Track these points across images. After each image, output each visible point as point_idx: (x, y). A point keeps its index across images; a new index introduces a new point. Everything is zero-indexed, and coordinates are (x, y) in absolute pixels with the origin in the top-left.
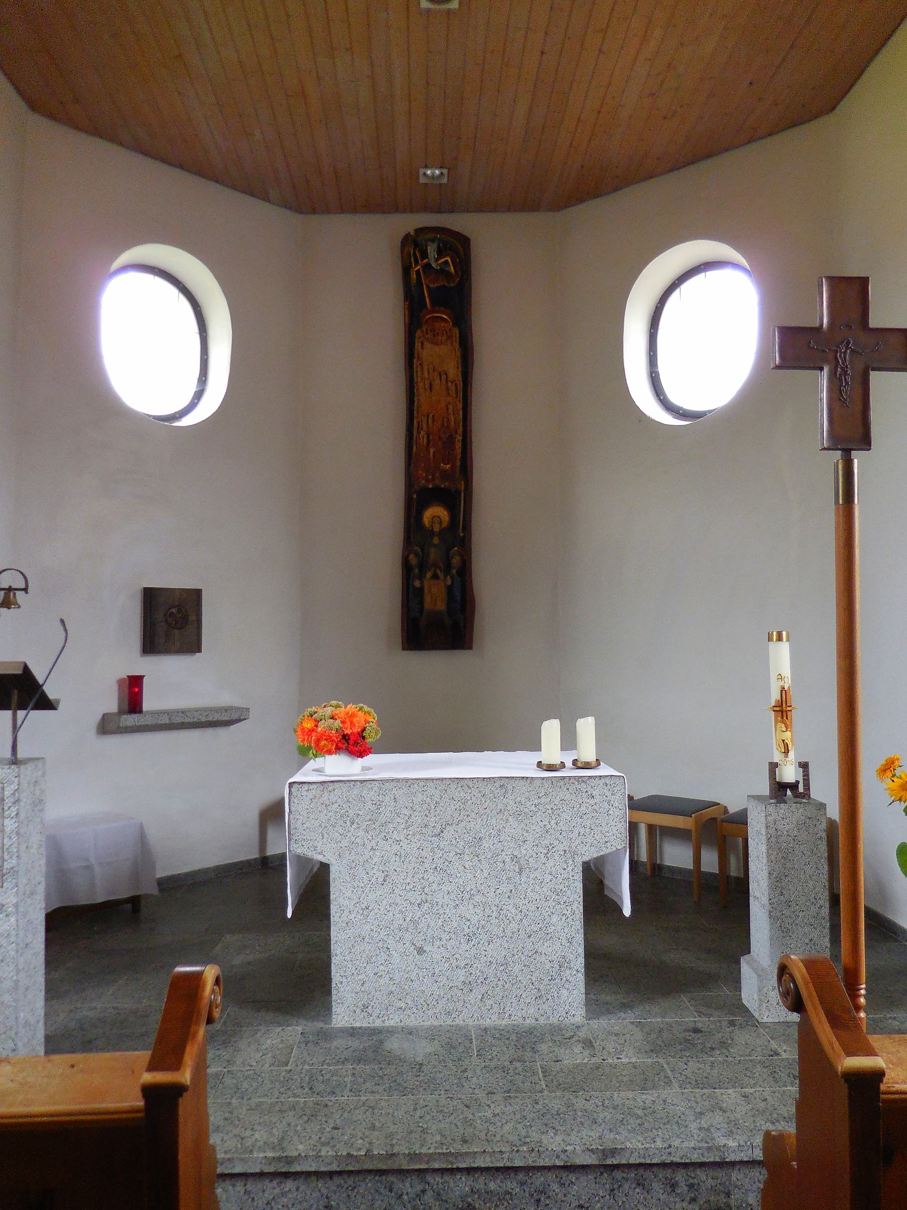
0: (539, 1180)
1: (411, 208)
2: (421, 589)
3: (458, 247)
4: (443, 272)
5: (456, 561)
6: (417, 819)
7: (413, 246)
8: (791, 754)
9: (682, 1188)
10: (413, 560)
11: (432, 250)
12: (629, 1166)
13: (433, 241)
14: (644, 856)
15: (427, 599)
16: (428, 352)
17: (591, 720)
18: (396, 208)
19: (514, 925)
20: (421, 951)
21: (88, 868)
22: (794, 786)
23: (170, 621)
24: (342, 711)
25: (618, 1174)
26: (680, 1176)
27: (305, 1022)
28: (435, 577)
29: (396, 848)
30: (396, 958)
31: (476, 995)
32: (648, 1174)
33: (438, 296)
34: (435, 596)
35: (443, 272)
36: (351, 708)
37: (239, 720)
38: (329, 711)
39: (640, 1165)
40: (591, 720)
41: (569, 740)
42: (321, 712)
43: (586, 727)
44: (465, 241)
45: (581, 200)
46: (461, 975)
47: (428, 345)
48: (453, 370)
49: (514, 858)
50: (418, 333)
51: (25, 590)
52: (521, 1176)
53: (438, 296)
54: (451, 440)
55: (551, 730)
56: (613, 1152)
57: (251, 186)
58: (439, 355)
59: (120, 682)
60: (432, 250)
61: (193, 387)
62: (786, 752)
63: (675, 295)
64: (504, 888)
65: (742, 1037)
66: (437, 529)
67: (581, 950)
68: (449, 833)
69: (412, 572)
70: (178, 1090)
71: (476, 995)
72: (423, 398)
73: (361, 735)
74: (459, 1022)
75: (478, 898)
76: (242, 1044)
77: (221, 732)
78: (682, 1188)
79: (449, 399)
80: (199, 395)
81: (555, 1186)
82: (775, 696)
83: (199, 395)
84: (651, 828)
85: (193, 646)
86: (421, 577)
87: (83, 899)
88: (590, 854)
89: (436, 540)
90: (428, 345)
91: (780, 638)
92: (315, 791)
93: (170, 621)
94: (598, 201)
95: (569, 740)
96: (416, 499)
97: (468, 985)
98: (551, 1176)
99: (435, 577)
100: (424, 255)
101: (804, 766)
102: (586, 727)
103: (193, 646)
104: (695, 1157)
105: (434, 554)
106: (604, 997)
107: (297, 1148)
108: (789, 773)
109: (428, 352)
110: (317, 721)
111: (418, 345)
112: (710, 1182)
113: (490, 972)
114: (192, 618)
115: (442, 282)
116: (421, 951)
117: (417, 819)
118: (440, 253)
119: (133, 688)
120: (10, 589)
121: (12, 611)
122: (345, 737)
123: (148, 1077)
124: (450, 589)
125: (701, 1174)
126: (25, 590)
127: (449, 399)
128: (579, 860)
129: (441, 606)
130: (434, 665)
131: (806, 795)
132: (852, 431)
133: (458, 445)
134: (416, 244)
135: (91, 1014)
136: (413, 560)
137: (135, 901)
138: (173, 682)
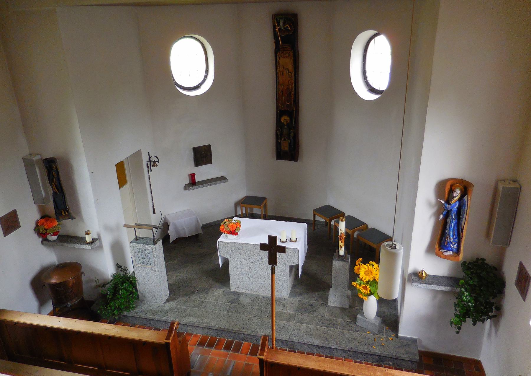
4: (286, 29)
5: (292, 134)
6: (248, 252)
7: (276, 18)
13: (281, 18)
15: (282, 147)
16: (282, 61)
20: (250, 279)
21: (184, 229)
23: (202, 155)
27: (225, 288)
28: (285, 140)
30: (244, 280)
31: (263, 289)
33: (287, 37)
34: (285, 146)
46: (259, 285)
48: (290, 67)
50: (278, 54)
51: (158, 162)
53: (287, 37)
54: (290, 93)
59: (189, 175)
60: (281, 22)
61: (204, 74)
63: (373, 41)
65: (321, 310)
68: (255, 256)
69: (279, 136)
70: (169, 343)
71: (263, 289)
76: (210, 293)
79: (290, 79)
80: (206, 77)
83: (206, 77)
85: (210, 161)
86: (281, 139)
87: (183, 236)
89: (286, 127)
93: (202, 155)
96: (280, 113)
97: (261, 287)
99: (285, 140)
103: (210, 161)
105: (285, 131)
106: (298, 291)
107: (212, 324)
109: (282, 61)
111: (278, 59)
113: (266, 285)
116: (250, 279)
117: (248, 252)
118: (285, 23)
119: (193, 176)
121: (156, 167)
122: (231, 232)
123: (165, 341)
124: (290, 143)
126: (158, 162)
127: (290, 79)
129: (287, 149)
135: (181, 278)
136: (279, 134)
137: (197, 236)
138: (204, 172)
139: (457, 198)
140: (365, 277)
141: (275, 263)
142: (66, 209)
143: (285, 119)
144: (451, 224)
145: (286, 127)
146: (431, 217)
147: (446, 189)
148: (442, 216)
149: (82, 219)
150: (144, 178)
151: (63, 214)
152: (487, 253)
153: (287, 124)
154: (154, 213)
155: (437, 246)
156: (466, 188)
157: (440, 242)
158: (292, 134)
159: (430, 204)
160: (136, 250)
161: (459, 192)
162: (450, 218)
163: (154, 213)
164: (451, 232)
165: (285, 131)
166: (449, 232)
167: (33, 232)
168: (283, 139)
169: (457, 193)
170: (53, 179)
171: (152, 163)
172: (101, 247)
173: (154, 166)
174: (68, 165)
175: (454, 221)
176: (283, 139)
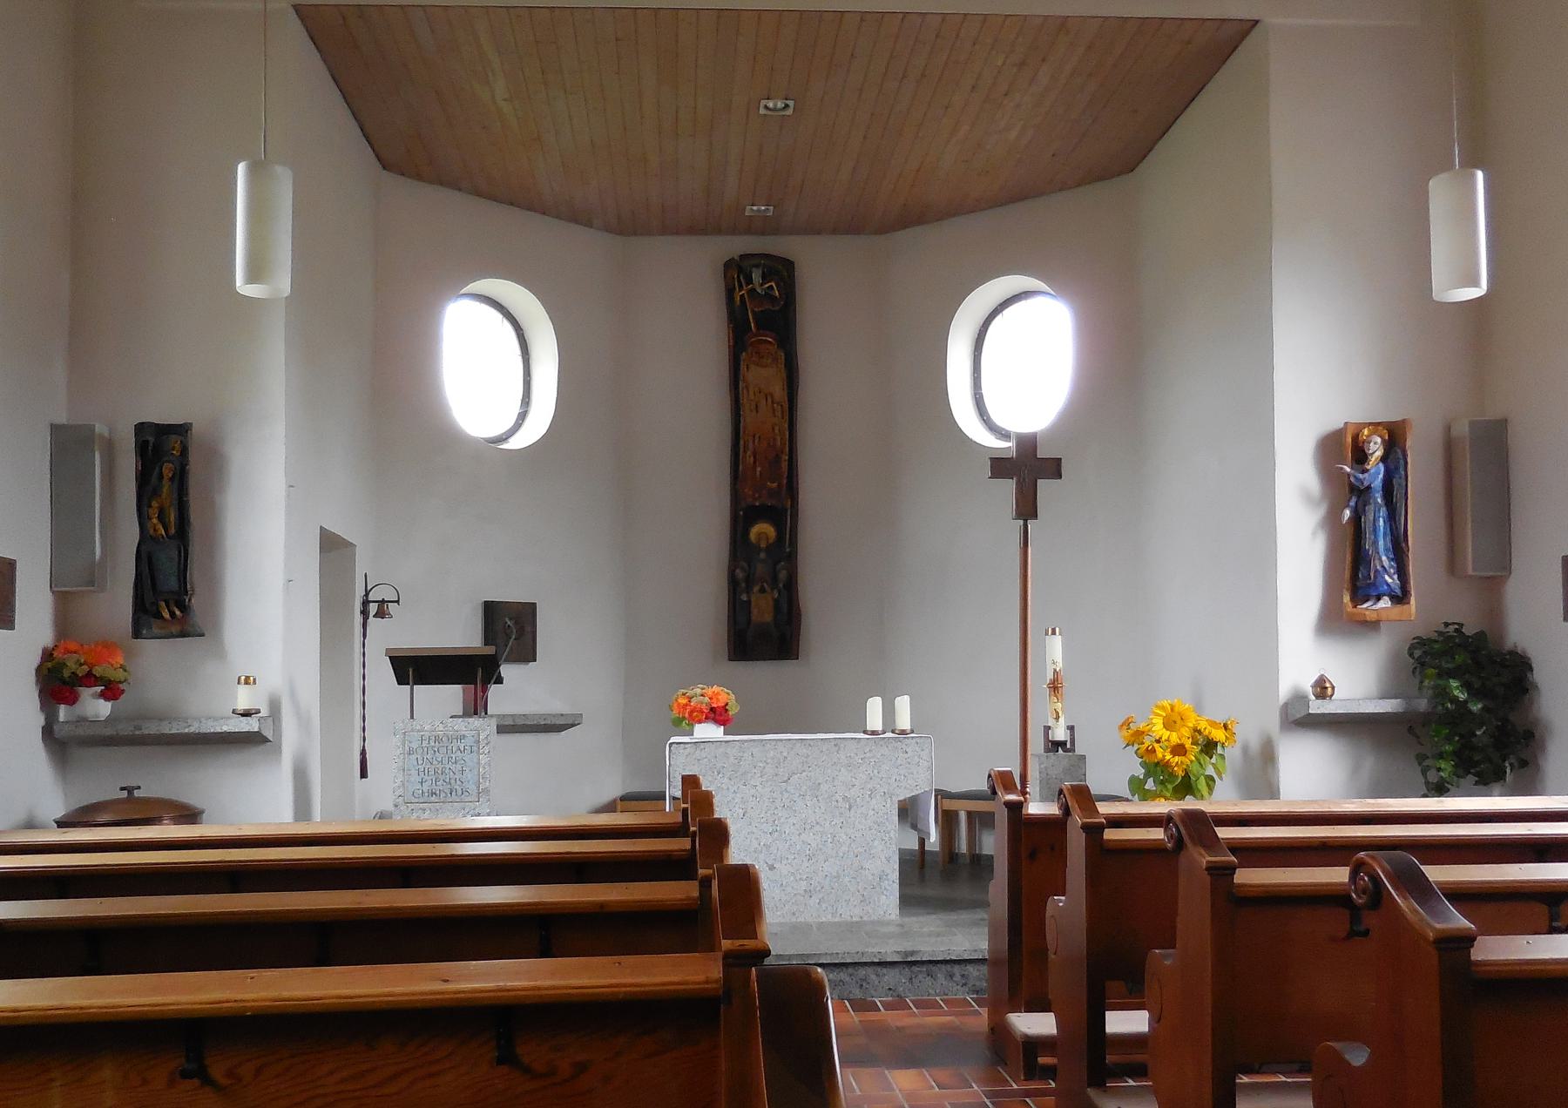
0: (862, 972)
1: (734, 231)
2: (749, 602)
3: (782, 271)
4: (768, 296)
5: (783, 575)
7: (736, 271)
8: (1062, 720)
9: (957, 978)
10: (740, 574)
11: (756, 276)
12: (923, 962)
13: (757, 266)
14: (963, 847)
15: (755, 611)
17: (906, 698)
18: (718, 231)
19: (844, 848)
22: (1062, 744)
24: (709, 691)
25: (916, 969)
26: (957, 969)
28: (762, 590)
29: (753, 791)
31: (815, 900)
32: (934, 968)
33: (761, 317)
34: (762, 608)
35: (768, 296)
36: (716, 688)
37: (573, 725)
38: (698, 691)
39: (930, 962)
40: (906, 698)
41: (889, 713)
42: (690, 693)
43: (903, 704)
44: (789, 265)
45: (905, 227)
47: (752, 367)
48: (779, 391)
49: (845, 798)
52: (850, 970)
53: (761, 317)
54: (778, 458)
55: (875, 707)
56: (912, 953)
57: (577, 216)
58: (764, 377)
60: (756, 276)
61: (516, 409)
62: (1057, 718)
64: (837, 821)
66: (763, 545)
67: (897, 866)
69: (737, 589)
71: (815, 900)
72: (748, 417)
73: (725, 709)
74: (801, 919)
75: (817, 828)
77: (553, 737)
78: (957, 978)
80: (522, 416)
81: (873, 977)
82: (1050, 676)
83: (522, 416)
84: (969, 814)
86: (748, 590)
88: (905, 794)
89: (762, 555)
90: (752, 367)
91: (1054, 633)
92: (689, 749)
94: (918, 229)
95: (889, 713)
96: (742, 516)
97: (809, 893)
98: (870, 970)
99: (762, 590)
100: (749, 280)
101: (1071, 728)
102: (903, 704)
104: (966, 957)
105: (760, 569)
108: (1060, 734)
110: (690, 698)
111: (743, 367)
112: (976, 973)
114: (528, 629)
115: (768, 306)
118: (765, 278)
120: (383, 601)
122: (712, 709)
124: (777, 602)
125: (970, 968)
128: (896, 800)
129: (768, 618)
130: (762, 674)
131: (1072, 750)
132: (1027, 509)
133: (785, 465)
134: (740, 270)
136: (740, 574)
139: (1379, 453)
140: (1166, 734)
141: (1034, 514)
142: (180, 599)
143: (762, 530)
144: (1375, 520)
145: (762, 555)
146: (1314, 534)
147: (1341, 452)
148: (1347, 513)
149: (219, 652)
150: (352, 648)
151: (166, 615)
152: (1463, 612)
153: (769, 549)
154: (364, 774)
155: (1347, 598)
156: (1394, 437)
157: (1355, 578)
158: (783, 575)
159: (1308, 498)
160: (415, 745)
161: (1379, 440)
162: (1370, 509)
163: (364, 774)
164: (1381, 543)
165: (760, 569)
166: (1375, 543)
167: (32, 678)
168: (756, 589)
169: (1376, 449)
170: (156, 493)
171: (373, 608)
172: (278, 750)
173: (381, 614)
174: (216, 460)
175: (1383, 512)
176: (756, 589)
